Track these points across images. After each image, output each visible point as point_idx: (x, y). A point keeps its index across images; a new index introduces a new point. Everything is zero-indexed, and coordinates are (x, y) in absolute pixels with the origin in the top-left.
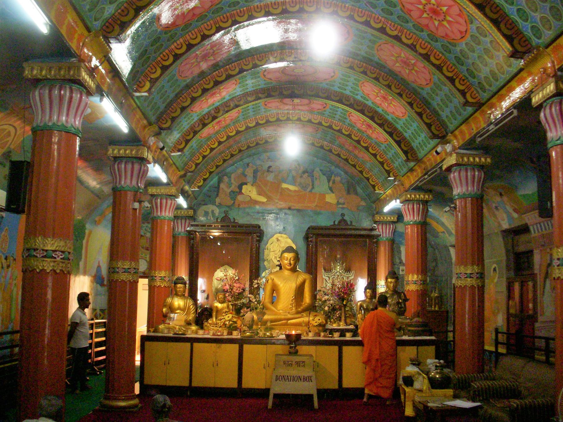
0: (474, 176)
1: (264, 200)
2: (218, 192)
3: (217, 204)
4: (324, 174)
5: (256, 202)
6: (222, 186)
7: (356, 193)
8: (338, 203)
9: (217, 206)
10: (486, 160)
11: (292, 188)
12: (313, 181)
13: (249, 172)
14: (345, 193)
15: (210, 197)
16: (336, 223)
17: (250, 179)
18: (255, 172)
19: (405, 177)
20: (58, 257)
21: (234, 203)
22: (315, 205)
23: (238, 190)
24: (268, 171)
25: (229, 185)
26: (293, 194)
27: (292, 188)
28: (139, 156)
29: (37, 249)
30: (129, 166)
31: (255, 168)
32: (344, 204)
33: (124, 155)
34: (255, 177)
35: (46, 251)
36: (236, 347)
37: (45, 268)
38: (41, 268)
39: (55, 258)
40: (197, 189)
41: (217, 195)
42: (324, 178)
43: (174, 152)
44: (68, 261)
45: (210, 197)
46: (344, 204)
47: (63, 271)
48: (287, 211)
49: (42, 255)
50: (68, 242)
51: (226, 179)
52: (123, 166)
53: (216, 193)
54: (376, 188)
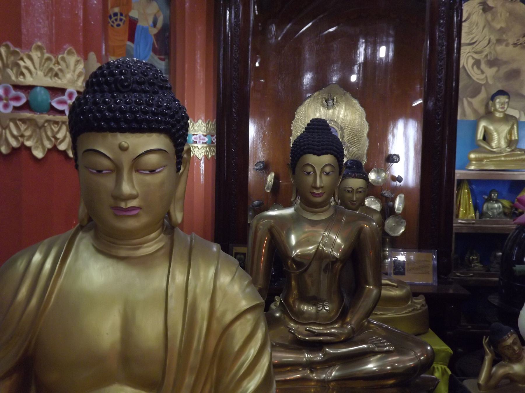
37: (28, 144)
38: (14, 144)
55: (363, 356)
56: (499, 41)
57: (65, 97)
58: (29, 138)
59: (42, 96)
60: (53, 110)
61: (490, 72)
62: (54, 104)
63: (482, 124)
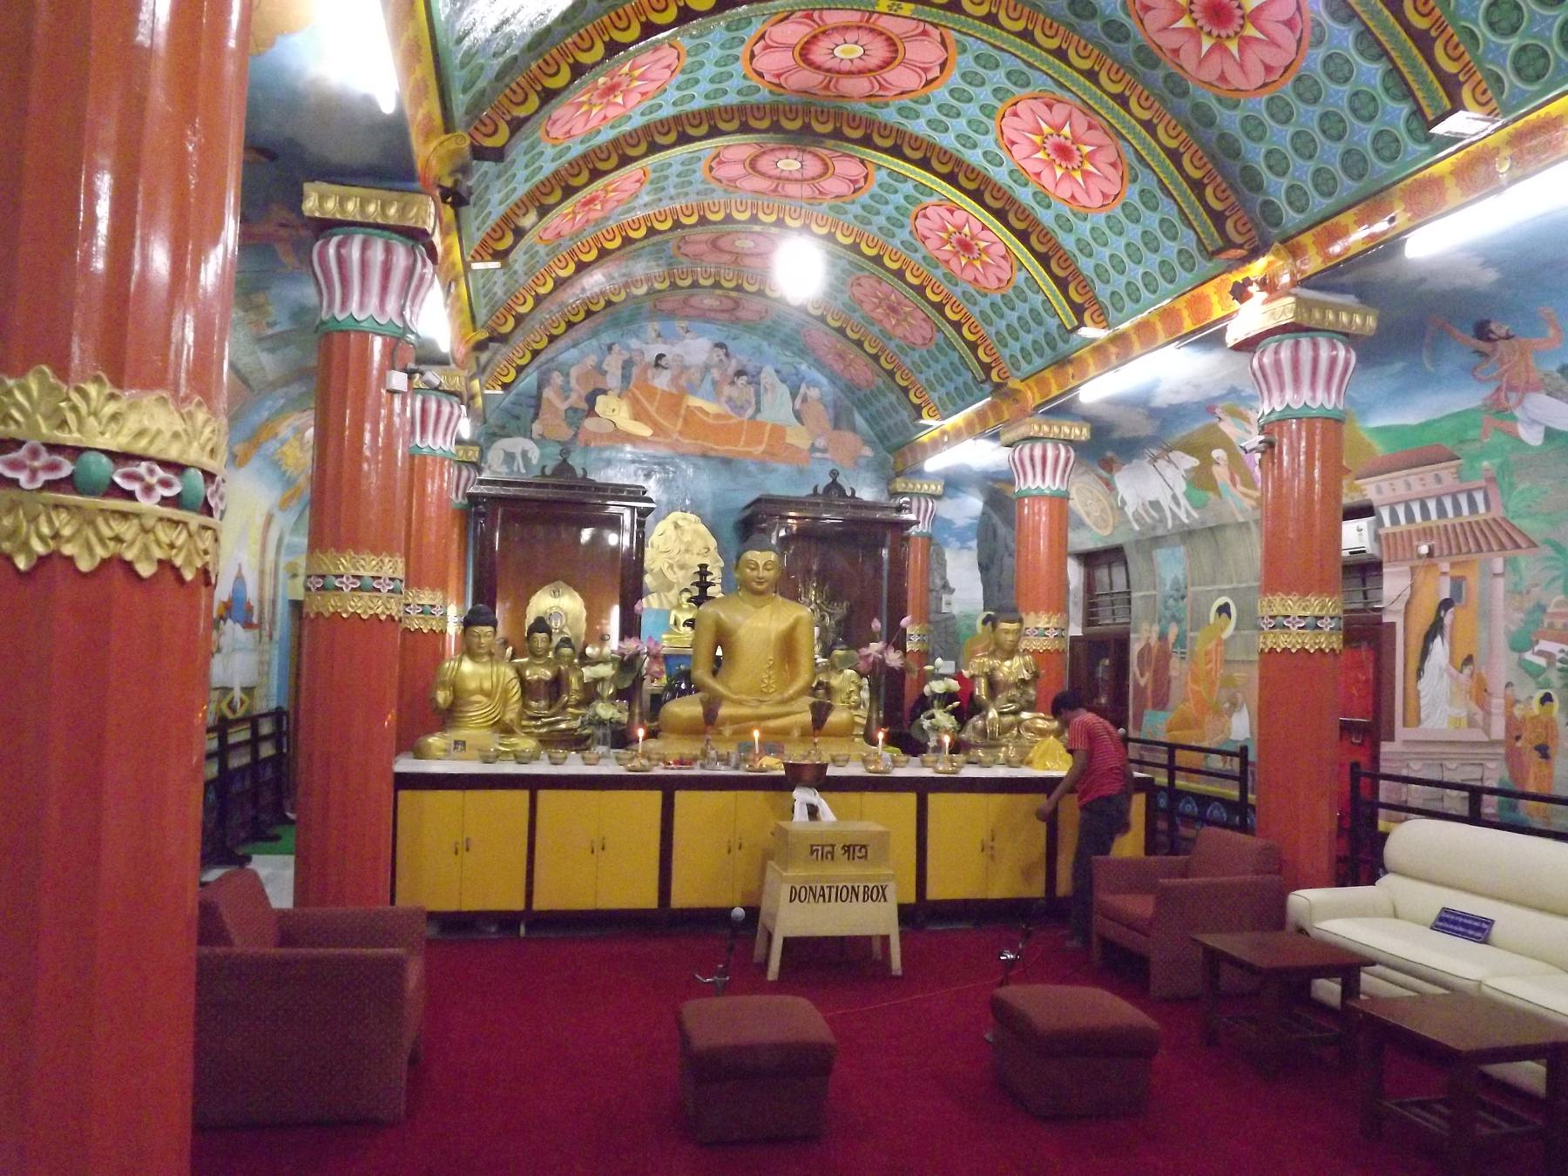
0: (1333, 362)
1: (645, 431)
2: (538, 407)
3: (534, 435)
4: (783, 381)
5: (630, 438)
6: (548, 393)
7: (854, 429)
8: (813, 448)
9: (536, 442)
10: (1364, 320)
11: (711, 408)
12: (758, 395)
13: (613, 364)
14: (828, 426)
15: (518, 418)
16: (820, 491)
17: (613, 380)
18: (627, 365)
19: (1031, 382)
20: (148, 490)
21: (576, 435)
22: (761, 448)
23: (585, 406)
24: (657, 365)
25: (565, 392)
26: (711, 421)
27: (711, 408)
28: (411, 223)
29: (19, 444)
30: (377, 254)
31: (626, 355)
32: (824, 451)
33: (359, 218)
34: (626, 377)
35: (76, 452)
36: (656, 797)
37: (68, 550)
38: (39, 548)
39: (130, 496)
40: (499, 391)
41: (536, 416)
42: (784, 390)
43: (483, 260)
44: (205, 520)
45: (518, 418)
46: (824, 451)
47: (176, 571)
48: (701, 462)
49: (43, 477)
50: (201, 416)
51: (557, 378)
52: (355, 253)
53: (532, 411)
54: (924, 412)
55: (558, 722)
56: (687, 551)
57: (21, 454)
58: (69, 540)
59: (369, 581)
60: (114, 491)
61: (681, 573)
62: (118, 480)
63: (673, 613)
